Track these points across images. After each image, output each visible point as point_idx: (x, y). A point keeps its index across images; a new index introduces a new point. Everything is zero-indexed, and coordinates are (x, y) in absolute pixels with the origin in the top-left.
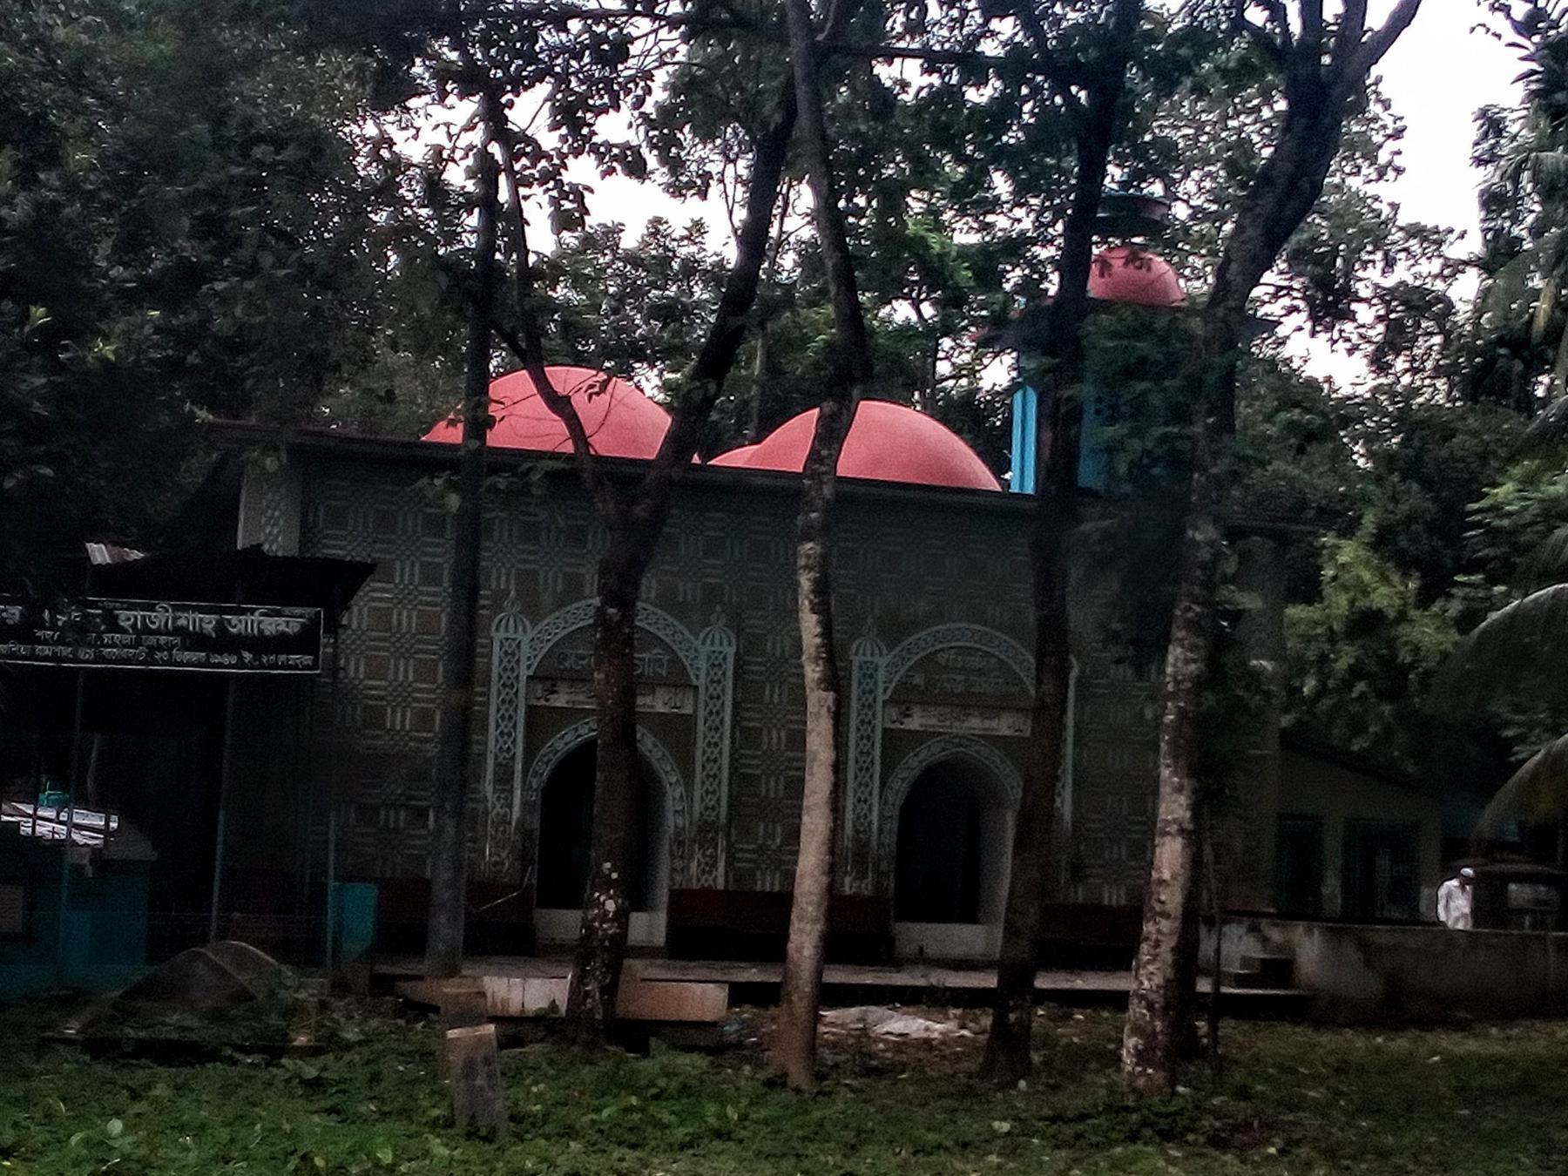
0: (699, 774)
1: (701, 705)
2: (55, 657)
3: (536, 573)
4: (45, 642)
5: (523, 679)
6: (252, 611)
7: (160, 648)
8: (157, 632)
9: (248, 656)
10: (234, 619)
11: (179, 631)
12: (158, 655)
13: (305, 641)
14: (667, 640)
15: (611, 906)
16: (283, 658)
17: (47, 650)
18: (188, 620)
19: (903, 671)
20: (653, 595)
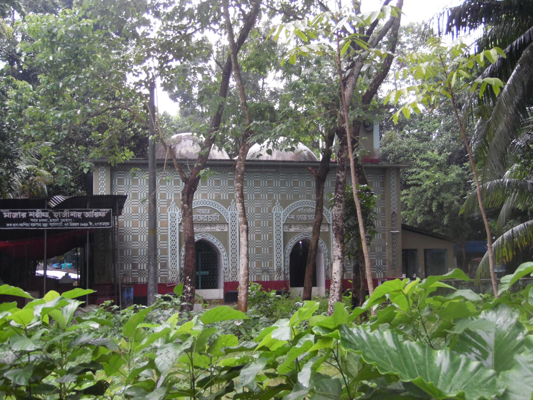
0: (230, 249)
1: (230, 228)
2: (36, 226)
4: (34, 222)
5: (177, 225)
6: (92, 211)
7: (66, 222)
8: (65, 218)
9: (91, 223)
10: (87, 213)
11: (71, 217)
12: (65, 224)
13: (107, 218)
14: (219, 210)
15: (189, 289)
16: (101, 223)
17: (34, 225)
18: (73, 214)
19: (288, 215)
20: (214, 198)
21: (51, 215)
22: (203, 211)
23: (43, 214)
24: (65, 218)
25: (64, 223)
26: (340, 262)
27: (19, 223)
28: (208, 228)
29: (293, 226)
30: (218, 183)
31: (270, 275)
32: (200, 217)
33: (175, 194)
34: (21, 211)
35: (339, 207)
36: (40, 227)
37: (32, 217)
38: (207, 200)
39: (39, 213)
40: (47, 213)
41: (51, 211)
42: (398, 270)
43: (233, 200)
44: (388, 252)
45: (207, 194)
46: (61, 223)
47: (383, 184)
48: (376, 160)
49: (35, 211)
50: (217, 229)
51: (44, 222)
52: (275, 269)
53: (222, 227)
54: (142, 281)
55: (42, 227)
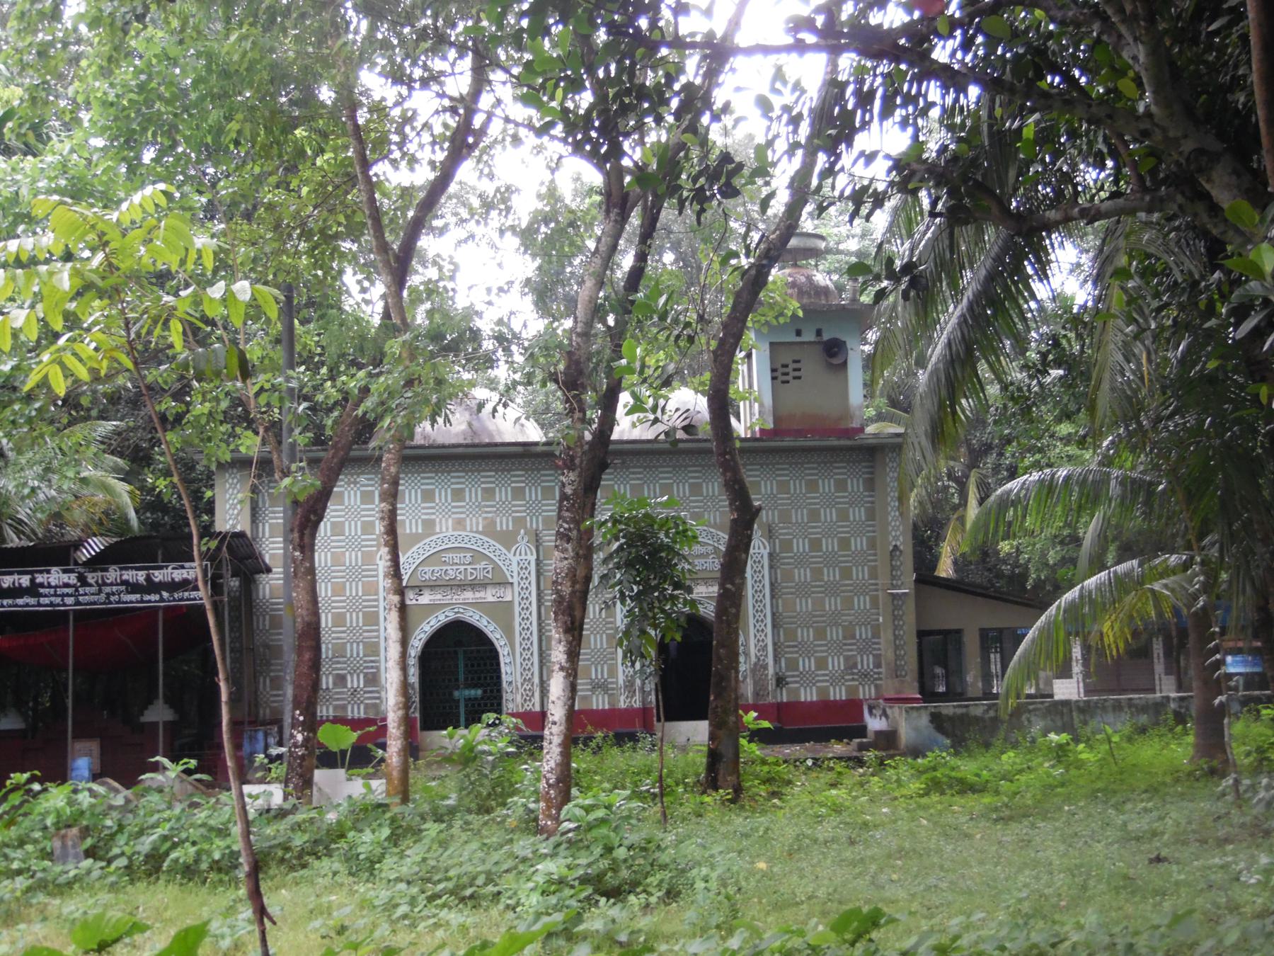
0: (518, 639)
2: (51, 604)
4: (46, 596)
6: (167, 567)
7: (113, 594)
8: (112, 584)
9: (165, 594)
10: (156, 573)
12: (112, 598)
14: (491, 555)
15: (300, 737)
16: (186, 594)
18: (129, 575)
20: (481, 529)
21: (83, 580)
22: (456, 557)
23: (65, 578)
24: (112, 584)
25: (108, 595)
26: (565, 677)
27: (14, 597)
28: (469, 595)
29: (426, 593)
30: (489, 493)
31: (610, 695)
32: (450, 572)
33: (423, 521)
34: (20, 573)
35: (564, 551)
36: (58, 605)
37: (42, 585)
38: (464, 534)
39: (56, 576)
40: (73, 576)
41: (81, 570)
42: (908, 678)
43: (522, 531)
44: (886, 636)
45: (464, 519)
46: (103, 596)
47: (870, 485)
48: (853, 429)
49: (48, 572)
50: (489, 596)
51: (68, 595)
52: (621, 682)
53: (500, 592)
54: (325, 713)
55: (64, 605)
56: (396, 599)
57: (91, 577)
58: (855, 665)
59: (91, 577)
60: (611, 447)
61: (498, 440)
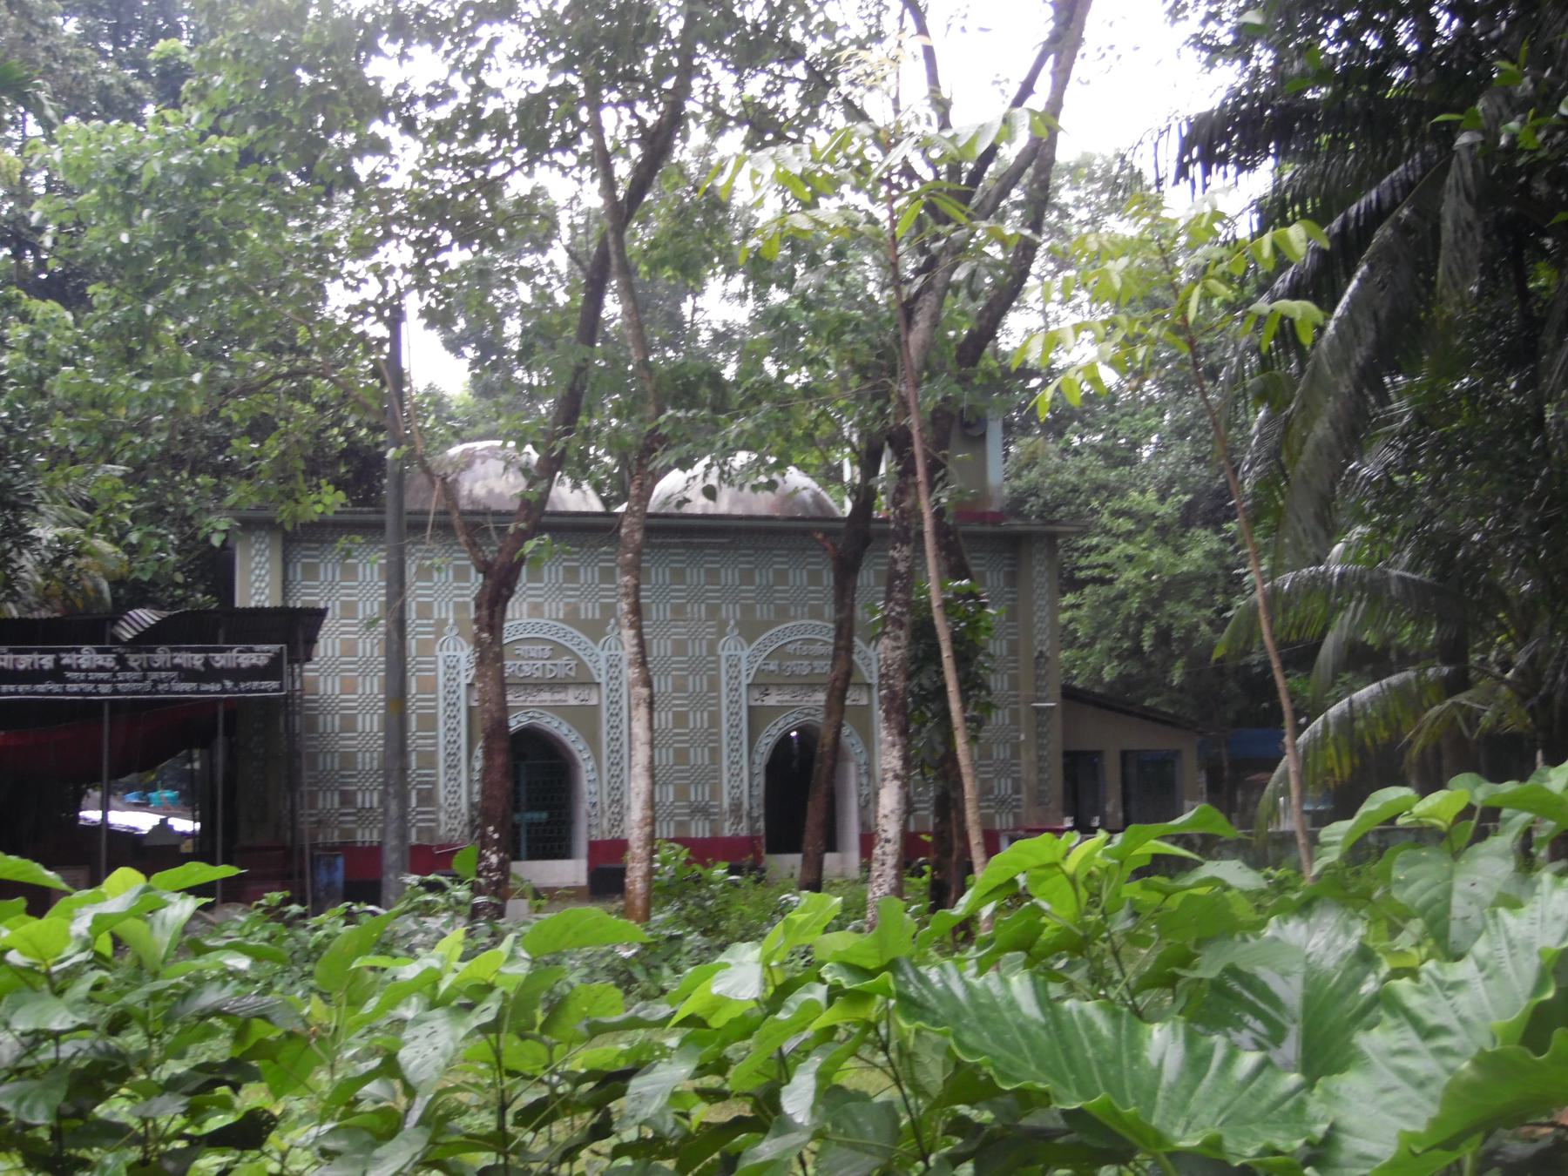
0: (605, 752)
2: (81, 692)
3: (354, 604)
8: (159, 669)
9: (229, 684)
10: (218, 656)
11: (176, 667)
13: (272, 670)
15: (494, 859)
18: (182, 659)
21: (122, 662)
22: (534, 650)
23: (100, 660)
24: (159, 669)
25: (155, 682)
28: (546, 697)
29: (773, 691)
35: (897, 638)
37: (69, 668)
39: (87, 657)
44: (1027, 757)
47: (1012, 579)
49: (78, 651)
50: (571, 698)
56: (645, 692)
57: (133, 660)
58: (991, 790)
59: (133, 660)
60: (873, 526)
61: (561, 508)
